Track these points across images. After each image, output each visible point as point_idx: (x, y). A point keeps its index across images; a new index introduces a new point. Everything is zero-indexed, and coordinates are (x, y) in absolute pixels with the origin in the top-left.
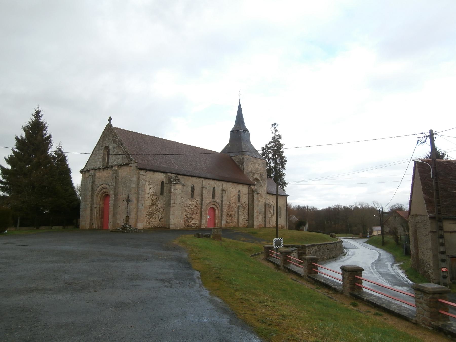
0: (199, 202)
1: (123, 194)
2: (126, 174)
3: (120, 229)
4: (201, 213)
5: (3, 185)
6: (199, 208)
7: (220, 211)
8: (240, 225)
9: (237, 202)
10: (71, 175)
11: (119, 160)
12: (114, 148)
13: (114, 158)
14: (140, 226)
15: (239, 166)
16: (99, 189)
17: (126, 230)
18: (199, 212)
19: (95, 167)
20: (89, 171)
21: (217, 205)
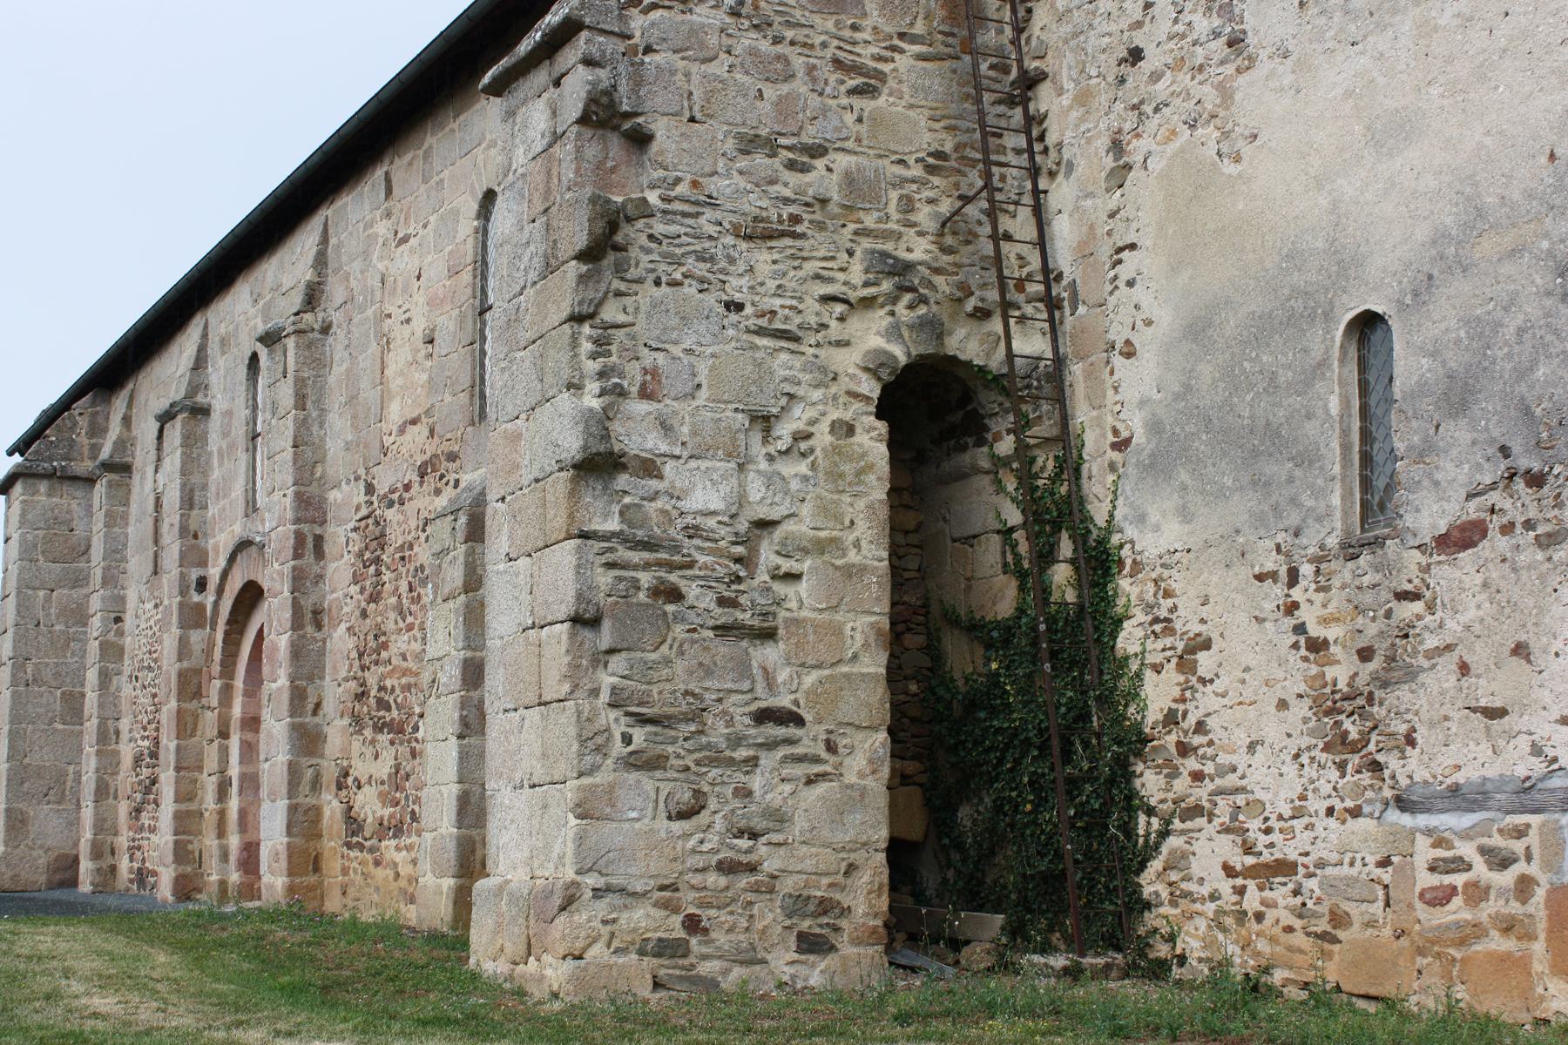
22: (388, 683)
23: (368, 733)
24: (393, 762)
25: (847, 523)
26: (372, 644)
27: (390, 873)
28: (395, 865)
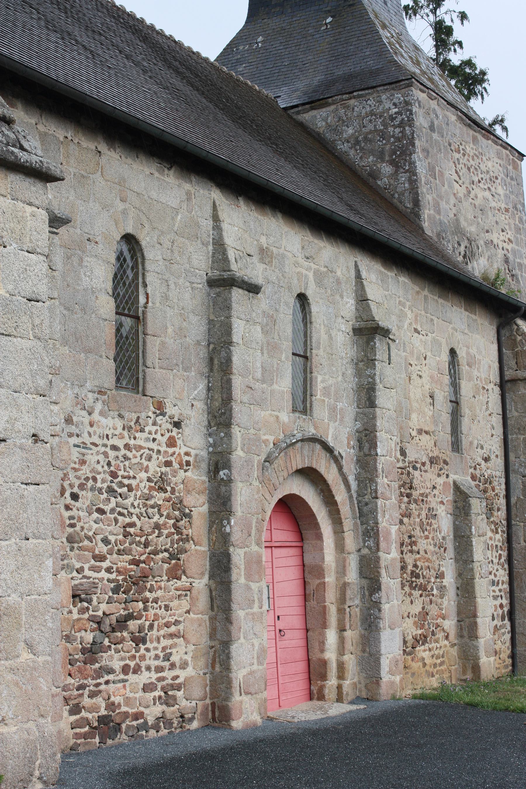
0: (194, 441)
4: (220, 566)
5: (362, 707)
6: (199, 506)
7: (351, 541)
8: (386, 677)
9: (448, 454)
15: (374, 175)
21: (331, 474)
22: (418, 563)
23: (407, 589)
24: (422, 606)
25: (140, 227)
26: (407, 540)
27: (420, 664)
28: (423, 659)
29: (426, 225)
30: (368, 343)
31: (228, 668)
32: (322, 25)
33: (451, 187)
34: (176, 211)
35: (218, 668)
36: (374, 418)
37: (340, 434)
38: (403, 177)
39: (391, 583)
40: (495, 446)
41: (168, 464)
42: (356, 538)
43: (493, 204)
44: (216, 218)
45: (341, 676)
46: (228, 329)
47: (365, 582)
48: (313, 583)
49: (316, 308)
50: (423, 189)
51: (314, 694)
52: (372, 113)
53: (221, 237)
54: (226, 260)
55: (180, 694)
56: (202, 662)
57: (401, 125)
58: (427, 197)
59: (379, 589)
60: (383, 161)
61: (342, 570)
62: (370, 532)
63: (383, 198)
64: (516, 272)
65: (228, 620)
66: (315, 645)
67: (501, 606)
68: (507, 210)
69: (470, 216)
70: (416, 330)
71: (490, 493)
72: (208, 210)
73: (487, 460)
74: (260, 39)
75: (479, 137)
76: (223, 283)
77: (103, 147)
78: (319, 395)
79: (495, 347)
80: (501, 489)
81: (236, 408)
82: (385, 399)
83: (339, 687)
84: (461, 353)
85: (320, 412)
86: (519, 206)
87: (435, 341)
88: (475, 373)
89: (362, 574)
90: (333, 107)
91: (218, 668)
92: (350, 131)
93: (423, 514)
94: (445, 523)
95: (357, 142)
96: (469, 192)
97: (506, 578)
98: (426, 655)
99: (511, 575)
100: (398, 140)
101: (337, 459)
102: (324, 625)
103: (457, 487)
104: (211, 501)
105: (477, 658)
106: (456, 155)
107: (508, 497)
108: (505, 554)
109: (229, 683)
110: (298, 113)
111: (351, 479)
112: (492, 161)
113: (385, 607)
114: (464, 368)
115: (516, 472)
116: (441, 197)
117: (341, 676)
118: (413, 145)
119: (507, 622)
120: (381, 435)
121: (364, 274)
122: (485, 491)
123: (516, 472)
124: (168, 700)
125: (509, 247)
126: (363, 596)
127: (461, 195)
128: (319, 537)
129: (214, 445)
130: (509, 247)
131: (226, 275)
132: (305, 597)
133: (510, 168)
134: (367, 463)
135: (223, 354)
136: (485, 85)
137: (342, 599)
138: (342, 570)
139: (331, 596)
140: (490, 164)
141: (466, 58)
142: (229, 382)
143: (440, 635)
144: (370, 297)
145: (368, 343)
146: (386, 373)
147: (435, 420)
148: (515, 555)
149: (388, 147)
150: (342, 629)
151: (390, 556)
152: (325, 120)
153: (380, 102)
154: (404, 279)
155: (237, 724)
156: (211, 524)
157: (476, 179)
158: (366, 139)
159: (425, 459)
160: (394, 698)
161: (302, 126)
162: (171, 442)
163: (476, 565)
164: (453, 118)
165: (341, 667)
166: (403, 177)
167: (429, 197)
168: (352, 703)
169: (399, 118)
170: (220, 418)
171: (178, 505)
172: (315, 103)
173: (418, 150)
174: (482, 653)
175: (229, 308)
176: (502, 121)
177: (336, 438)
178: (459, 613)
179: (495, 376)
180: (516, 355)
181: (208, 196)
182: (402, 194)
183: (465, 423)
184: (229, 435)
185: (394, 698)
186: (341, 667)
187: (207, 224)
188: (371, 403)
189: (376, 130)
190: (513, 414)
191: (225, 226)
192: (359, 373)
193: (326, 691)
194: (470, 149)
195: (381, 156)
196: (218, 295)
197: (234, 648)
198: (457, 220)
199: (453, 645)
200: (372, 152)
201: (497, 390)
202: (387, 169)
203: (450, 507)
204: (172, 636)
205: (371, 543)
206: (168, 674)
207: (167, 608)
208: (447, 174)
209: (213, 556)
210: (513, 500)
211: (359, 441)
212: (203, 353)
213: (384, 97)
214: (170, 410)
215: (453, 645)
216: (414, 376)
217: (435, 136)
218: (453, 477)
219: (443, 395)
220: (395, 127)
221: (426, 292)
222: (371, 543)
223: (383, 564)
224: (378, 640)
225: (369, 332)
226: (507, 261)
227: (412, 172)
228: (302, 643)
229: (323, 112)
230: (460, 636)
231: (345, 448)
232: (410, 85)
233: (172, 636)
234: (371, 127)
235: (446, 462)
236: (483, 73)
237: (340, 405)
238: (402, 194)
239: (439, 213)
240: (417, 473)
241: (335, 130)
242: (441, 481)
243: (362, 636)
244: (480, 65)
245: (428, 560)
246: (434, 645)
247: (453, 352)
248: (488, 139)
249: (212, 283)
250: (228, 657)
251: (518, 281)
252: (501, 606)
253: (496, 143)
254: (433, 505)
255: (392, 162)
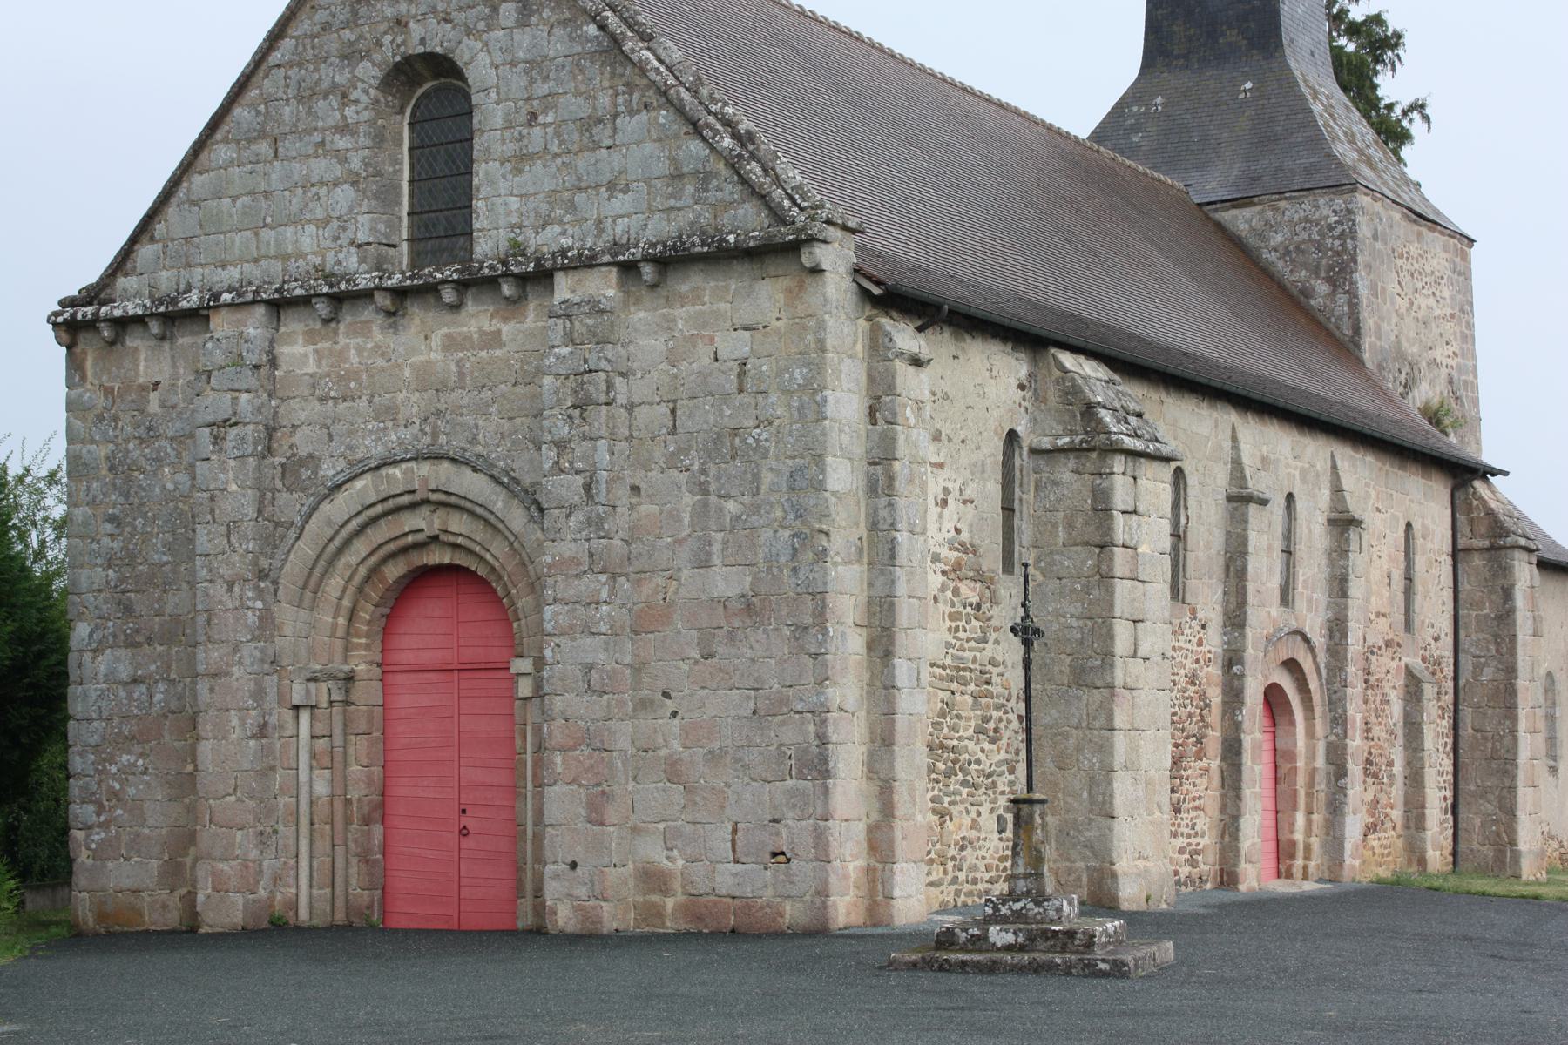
0: (1214, 641)
1: (703, 563)
2: (734, 345)
3: (1000, 936)
6: (1216, 696)
7: (1320, 729)
8: (1348, 861)
9: (1401, 636)
10: (947, 334)
11: (620, 203)
12: (536, 66)
13: (541, 177)
14: (915, 900)
15: (1307, 293)
16: (340, 507)
17: (588, 940)
18: (1214, 738)
19: (269, 274)
20: (177, 319)
21: (1307, 664)
29: (1366, 356)
30: (1342, 534)
31: (1236, 839)
32: (1239, 92)
33: (1393, 303)
34: (1208, 438)
35: (1227, 839)
36: (1346, 608)
37: (1314, 623)
38: (1342, 299)
39: (1355, 769)
40: (1445, 624)
41: (1197, 661)
42: (1324, 724)
43: (1438, 312)
44: (1234, 439)
45: (1307, 857)
46: (1244, 541)
47: (1332, 768)
48: (1285, 767)
49: (1300, 505)
50: (1364, 314)
51: (1283, 873)
52: (1306, 219)
53: (1239, 457)
54: (1243, 478)
55: (1200, 858)
56: (1214, 833)
57: (1342, 236)
58: (1368, 321)
59: (1345, 775)
60: (1318, 277)
61: (1312, 756)
62: (1339, 720)
63: (1318, 324)
64: (1461, 393)
65: (1238, 797)
66: (1284, 826)
67: (1445, 798)
68: (1452, 316)
69: (1412, 334)
70: (1378, 510)
71: (1439, 675)
72: (1229, 432)
73: (1436, 639)
74: (1159, 100)
75: (1424, 230)
76: (1241, 499)
77: (1164, 396)
78: (1300, 589)
79: (1449, 512)
80: (1449, 670)
81: (1250, 610)
82: (1356, 589)
83: (1305, 868)
84: (1416, 526)
85: (1301, 604)
86: (1467, 308)
87: (1394, 517)
88: (1429, 545)
89: (1329, 760)
90: (1258, 208)
91: (1227, 839)
92: (1279, 238)
93: (1379, 698)
94: (1396, 709)
95: (1287, 252)
96: (1412, 304)
97: (1451, 769)
98: (1376, 844)
99: (1455, 765)
100: (1338, 253)
101: (1312, 650)
102: (1295, 808)
103: (1409, 671)
104: (1224, 693)
105: (1423, 851)
106: (1400, 262)
107: (1456, 679)
108: (1450, 741)
109: (1238, 851)
110: (1216, 210)
111: (1322, 666)
112: (1438, 257)
113: (1350, 792)
114: (1419, 541)
115: (1467, 652)
116: (1382, 318)
117: (1307, 857)
118: (1356, 262)
119: (1449, 816)
120: (1352, 625)
121: (1339, 464)
122: (1434, 674)
123: (1467, 652)
124: (1193, 863)
125: (1453, 362)
126: (1329, 782)
127: (1403, 310)
128: (1292, 723)
129: (1228, 643)
130: (1453, 362)
131: (1244, 492)
132: (1276, 780)
133: (1458, 260)
134: (1338, 652)
135: (1239, 563)
136: (1400, 51)
137: (1311, 784)
138: (1312, 756)
139: (1301, 780)
140: (1434, 262)
141: (1373, 12)
142: (1244, 588)
143: (1388, 825)
144: (1345, 487)
145: (1342, 534)
146: (1356, 560)
147: (1391, 602)
148: (1461, 745)
149: (1324, 261)
150: (1309, 813)
151: (1355, 743)
152: (1249, 221)
153: (1317, 207)
154: (1370, 458)
155: (1242, 887)
156: (1224, 712)
157: (1419, 286)
158: (1297, 248)
159: (1381, 643)
160: (1354, 880)
161: (1219, 226)
162: (1200, 644)
163: (1426, 753)
164: (1397, 216)
165: (1308, 848)
166: (1342, 299)
167: (1370, 322)
168: (1320, 880)
169: (1340, 228)
170: (1235, 619)
171: (1203, 696)
172: (1236, 203)
173: (1361, 267)
174: (1429, 846)
175: (1246, 522)
176: (1422, 106)
177: (1311, 629)
178: (1406, 803)
179: (1448, 547)
180: (1471, 521)
181: (1231, 416)
182: (1340, 318)
183: (1418, 600)
184: (1243, 635)
185: (1354, 880)
186: (1308, 848)
187: (1228, 444)
188: (1344, 594)
189: (1310, 240)
190: (1465, 586)
191: (1242, 446)
192: (1332, 563)
193: (1294, 870)
194: (1414, 250)
195: (1316, 271)
196: (1236, 509)
197: (1242, 821)
198: (1399, 343)
199: (1399, 836)
200: (1304, 266)
201: (1449, 560)
202: (1322, 288)
203: (1401, 692)
204: (1197, 808)
205: (1339, 730)
206: (1193, 841)
207: (1194, 785)
208: (1389, 289)
209: (1225, 741)
210: (1462, 683)
211: (1330, 630)
212: (1222, 562)
213: (1322, 201)
214: (1200, 615)
215: (1399, 836)
216: (1375, 558)
217: (1379, 245)
218: (1405, 660)
219: (1398, 575)
220: (1334, 238)
221: (1387, 467)
222: (1339, 730)
223: (1349, 751)
224: (1342, 824)
225: (1343, 523)
226: (1451, 382)
227: (1353, 294)
228: (1273, 824)
229: (1246, 213)
230: (1407, 827)
231: (1319, 641)
232: (1354, 191)
233: (1197, 808)
234: (1305, 236)
235: (1399, 645)
236: (1398, 36)
237: (1315, 596)
238: (1340, 318)
239: (1379, 338)
240: (1374, 658)
241: (1261, 236)
242: (1394, 664)
243: (1326, 820)
244: (1393, 24)
245: (1381, 747)
246: (1382, 834)
247: (1409, 525)
248: (1434, 231)
249: (1230, 498)
250: (1237, 829)
251: (1462, 405)
252: (1445, 798)
253: (1443, 234)
254: (1387, 690)
255: (1329, 280)
